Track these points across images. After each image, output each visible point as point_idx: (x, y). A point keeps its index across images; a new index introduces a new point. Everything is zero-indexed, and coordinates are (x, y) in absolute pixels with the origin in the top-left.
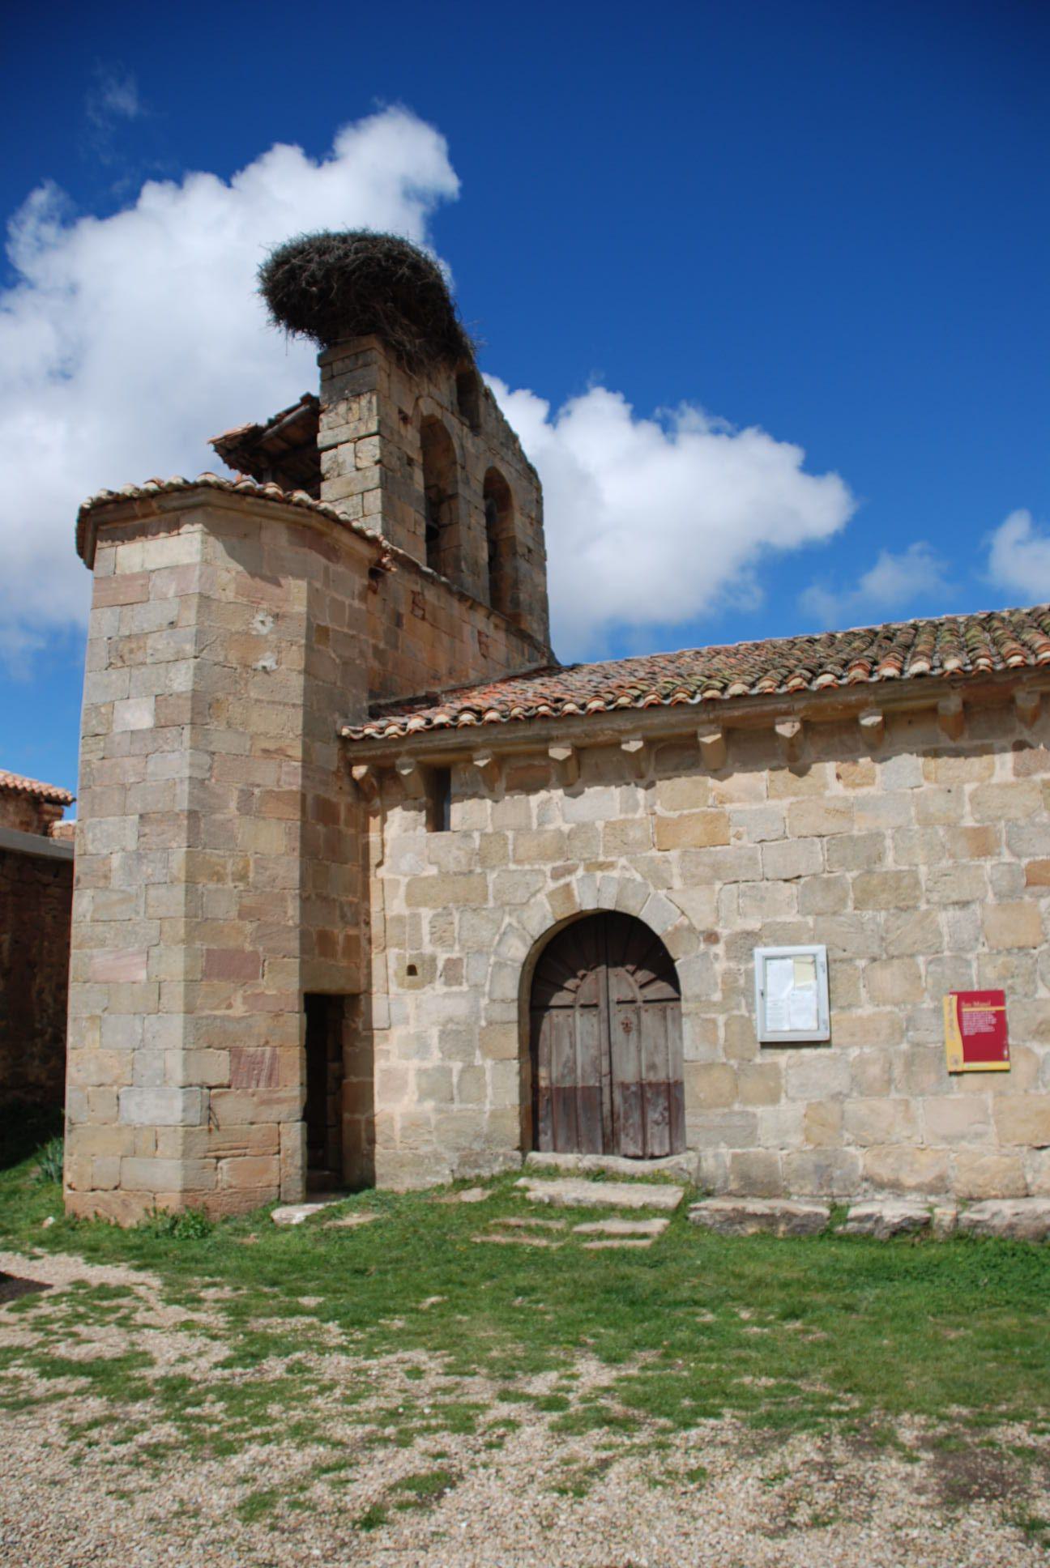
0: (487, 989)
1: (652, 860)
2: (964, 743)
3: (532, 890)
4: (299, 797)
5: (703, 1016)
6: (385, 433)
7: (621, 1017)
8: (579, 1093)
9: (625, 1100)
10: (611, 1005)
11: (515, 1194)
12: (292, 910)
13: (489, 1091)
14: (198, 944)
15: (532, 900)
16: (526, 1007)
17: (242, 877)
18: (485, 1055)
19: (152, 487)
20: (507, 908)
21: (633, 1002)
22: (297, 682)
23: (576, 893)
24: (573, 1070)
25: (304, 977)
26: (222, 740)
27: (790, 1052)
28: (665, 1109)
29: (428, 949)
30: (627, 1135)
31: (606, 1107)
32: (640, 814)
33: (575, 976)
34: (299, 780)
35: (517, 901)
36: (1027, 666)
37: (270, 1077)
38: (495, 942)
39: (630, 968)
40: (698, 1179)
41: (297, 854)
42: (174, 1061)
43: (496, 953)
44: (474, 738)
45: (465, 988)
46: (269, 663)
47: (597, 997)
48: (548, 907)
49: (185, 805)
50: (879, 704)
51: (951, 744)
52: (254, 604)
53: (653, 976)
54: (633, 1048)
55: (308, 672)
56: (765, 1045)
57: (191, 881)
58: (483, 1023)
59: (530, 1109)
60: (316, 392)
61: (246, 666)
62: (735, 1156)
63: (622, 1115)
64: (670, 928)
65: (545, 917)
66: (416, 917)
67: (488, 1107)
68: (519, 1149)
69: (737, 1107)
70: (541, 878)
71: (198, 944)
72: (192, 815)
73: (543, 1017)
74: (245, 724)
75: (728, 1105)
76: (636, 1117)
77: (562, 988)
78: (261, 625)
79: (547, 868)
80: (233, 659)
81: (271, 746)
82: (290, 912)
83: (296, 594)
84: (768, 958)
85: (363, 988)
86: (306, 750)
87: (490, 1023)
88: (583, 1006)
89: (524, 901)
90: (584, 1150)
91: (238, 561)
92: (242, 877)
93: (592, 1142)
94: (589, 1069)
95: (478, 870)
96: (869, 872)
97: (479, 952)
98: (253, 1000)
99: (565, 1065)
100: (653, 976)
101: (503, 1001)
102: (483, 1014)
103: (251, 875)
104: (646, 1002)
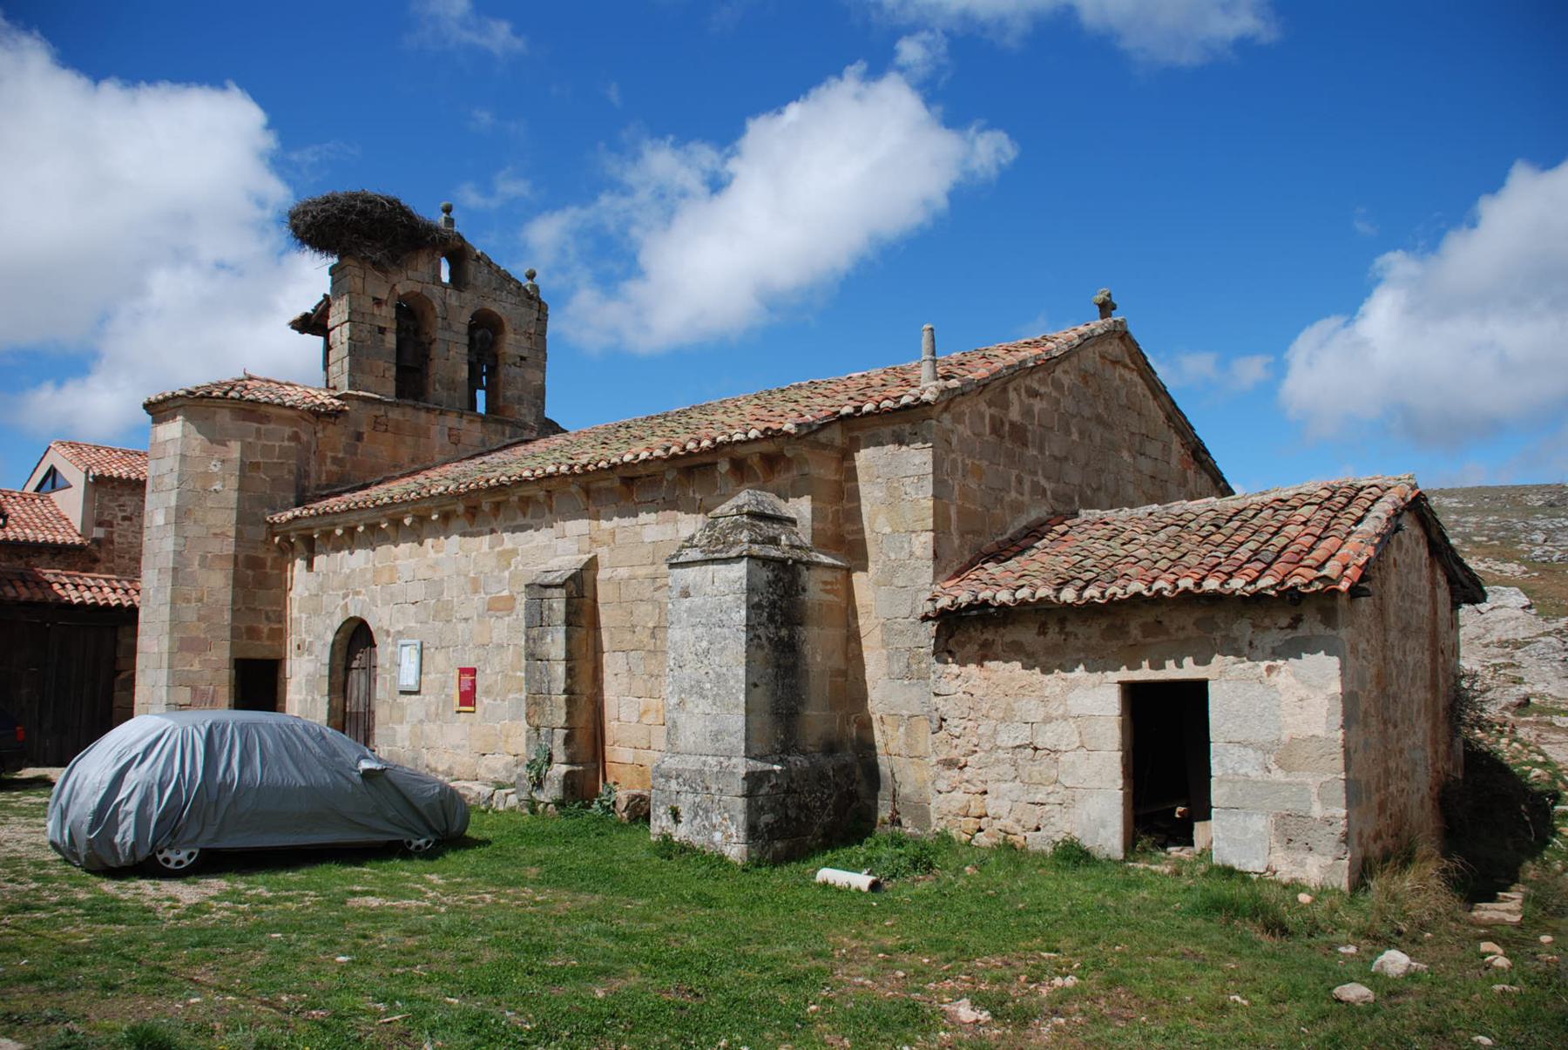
2: (475, 530)
4: (233, 557)
6: (357, 318)
12: (227, 616)
14: (176, 635)
17: (200, 600)
19: (160, 397)
22: (234, 496)
25: (232, 651)
26: (192, 530)
27: (408, 697)
29: (304, 636)
32: (370, 565)
34: (233, 548)
36: (432, 496)
37: (212, 701)
41: (230, 587)
42: (163, 692)
44: (312, 523)
45: (313, 657)
46: (218, 487)
49: (171, 565)
50: (437, 507)
51: (470, 530)
52: (210, 457)
55: (241, 489)
56: (402, 692)
57: (173, 602)
60: (328, 293)
61: (205, 490)
62: (389, 751)
66: (301, 617)
69: (390, 725)
71: (176, 635)
72: (174, 569)
74: (203, 521)
75: (388, 724)
78: (215, 467)
80: (198, 486)
81: (218, 531)
82: (226, 617)
83: (235, 450)
84: (403, 646)
85: (178, 656)
86: (239, 532)
91: (203, 434)
92: (200, 600)
96: (438, 600)
98: (204, 662)
103: (205, 599)
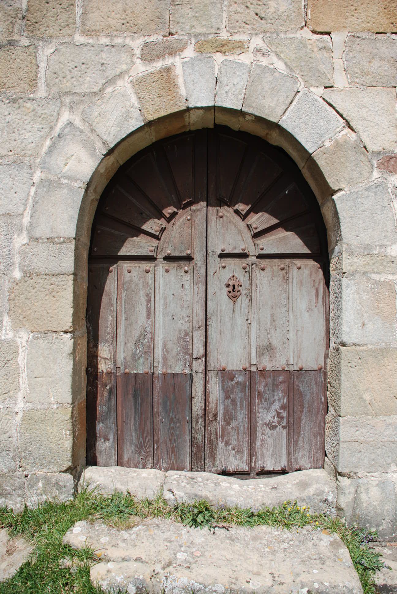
0: (26, 220)
1: (303, 43)
3: (110, 73)
5: (374, 277)
7: (225, 276)
8: (158, 384)
9: (227, 394)
10: (210, 258)
11: (66, 562)
13: (23, 380)
15: (109, 90)
16: (85, 254)
18: (17, 325)
20: (67, 100)
21: (243, 255)
23: (180, 82)
24: (150, 350)
28: (283, 407)
30: (227, 443)
31: (198, 404)
33: (160, 215)
35: (85, 89)
38: (45, 149)
39: (242, 207)
40: (355, 517)
43: (44, 166)
47: (191, 246)
48: (134, 100)
53: (274, 221)
54: (240, 321)
58: (17, 274)
59: (84, 404)
63: (221, 415)
64: (327, 144)
65: (127, 115)
67: (20, 405)
68: (68, 470)
70: (124, 57)
73: (109, 272)
76: (241, 418)
77: (138, 231)
79: (137, 44)
87: (28, 275)
88: (169, 258)
89: (96, 89)
90: (163, 463)
93: (175, 452)
94: (174, 349)
95: (25, 41)
97: (17, 163)
99: (137, 343)
100: (274, 221)
101: (50, 240)
102: (17, 260)
104: (261, 257)
